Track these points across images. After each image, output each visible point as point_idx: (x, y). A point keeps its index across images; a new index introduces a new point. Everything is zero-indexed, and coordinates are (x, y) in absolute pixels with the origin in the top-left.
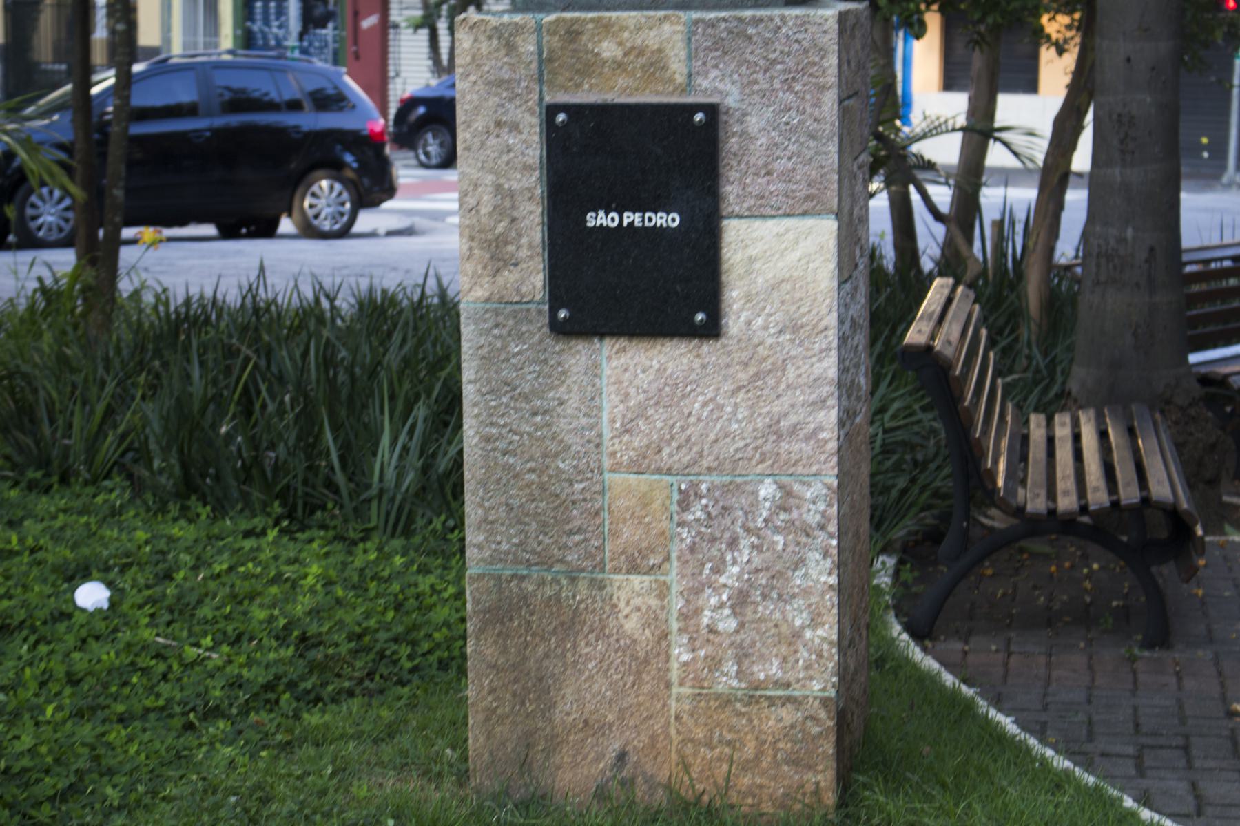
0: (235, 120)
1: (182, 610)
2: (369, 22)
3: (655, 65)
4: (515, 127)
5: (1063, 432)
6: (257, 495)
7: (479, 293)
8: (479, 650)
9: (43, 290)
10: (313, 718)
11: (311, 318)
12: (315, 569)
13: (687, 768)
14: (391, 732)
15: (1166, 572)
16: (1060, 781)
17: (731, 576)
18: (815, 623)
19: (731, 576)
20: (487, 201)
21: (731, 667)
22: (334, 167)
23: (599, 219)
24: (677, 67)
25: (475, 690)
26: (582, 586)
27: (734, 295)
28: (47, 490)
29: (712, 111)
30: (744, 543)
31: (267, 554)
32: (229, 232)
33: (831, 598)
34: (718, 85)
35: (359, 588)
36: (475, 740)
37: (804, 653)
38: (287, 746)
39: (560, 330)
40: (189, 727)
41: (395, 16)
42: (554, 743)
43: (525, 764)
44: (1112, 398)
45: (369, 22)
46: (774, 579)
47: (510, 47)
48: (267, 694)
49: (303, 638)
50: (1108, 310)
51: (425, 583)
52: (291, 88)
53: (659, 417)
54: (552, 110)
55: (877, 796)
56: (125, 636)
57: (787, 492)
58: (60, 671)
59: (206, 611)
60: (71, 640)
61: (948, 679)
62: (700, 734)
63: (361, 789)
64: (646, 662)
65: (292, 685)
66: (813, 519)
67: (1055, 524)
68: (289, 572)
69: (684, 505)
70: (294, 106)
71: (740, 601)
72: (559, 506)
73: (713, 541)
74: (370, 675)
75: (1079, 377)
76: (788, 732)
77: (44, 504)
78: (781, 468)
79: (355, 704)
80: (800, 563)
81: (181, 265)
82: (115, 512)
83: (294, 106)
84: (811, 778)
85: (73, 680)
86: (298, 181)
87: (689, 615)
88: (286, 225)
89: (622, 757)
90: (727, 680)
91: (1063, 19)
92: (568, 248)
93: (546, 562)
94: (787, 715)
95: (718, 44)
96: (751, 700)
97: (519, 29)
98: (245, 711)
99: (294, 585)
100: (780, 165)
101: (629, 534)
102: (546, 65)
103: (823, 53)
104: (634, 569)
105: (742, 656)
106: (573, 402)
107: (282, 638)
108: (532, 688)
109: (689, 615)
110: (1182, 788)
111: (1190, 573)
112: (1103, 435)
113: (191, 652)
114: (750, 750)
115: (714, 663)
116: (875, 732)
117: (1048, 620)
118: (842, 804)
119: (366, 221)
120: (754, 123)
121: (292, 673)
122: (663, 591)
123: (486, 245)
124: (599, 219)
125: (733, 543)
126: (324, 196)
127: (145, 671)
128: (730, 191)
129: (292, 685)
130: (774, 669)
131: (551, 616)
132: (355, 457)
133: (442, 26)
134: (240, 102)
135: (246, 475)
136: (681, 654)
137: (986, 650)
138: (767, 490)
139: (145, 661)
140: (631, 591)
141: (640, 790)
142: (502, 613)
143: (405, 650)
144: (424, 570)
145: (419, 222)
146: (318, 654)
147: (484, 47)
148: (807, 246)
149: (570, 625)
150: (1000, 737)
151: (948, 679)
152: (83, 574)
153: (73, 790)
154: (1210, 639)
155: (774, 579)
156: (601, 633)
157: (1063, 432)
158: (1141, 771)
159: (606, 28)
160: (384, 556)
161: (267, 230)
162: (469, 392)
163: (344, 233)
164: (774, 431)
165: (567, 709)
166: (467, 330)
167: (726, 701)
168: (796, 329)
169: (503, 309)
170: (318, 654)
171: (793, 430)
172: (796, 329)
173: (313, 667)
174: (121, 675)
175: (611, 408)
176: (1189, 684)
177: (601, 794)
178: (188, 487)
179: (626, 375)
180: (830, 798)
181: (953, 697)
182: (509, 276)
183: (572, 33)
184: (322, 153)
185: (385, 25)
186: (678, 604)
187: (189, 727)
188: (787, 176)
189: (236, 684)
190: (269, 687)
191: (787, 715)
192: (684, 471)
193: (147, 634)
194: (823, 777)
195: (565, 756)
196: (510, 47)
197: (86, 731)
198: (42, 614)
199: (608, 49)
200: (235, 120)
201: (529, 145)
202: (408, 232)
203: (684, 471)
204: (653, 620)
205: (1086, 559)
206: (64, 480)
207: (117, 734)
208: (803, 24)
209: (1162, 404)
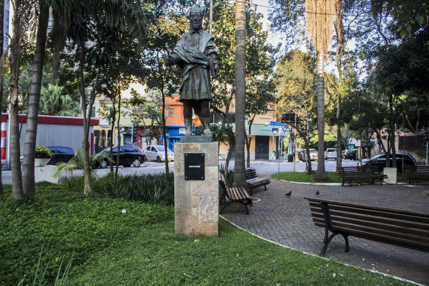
0: (125, 153)
1: (135, 213)
2: (139, 141)
3: (197, 149)
4: (181, 156)
5: (234, 190)
6: (140, 198)
7: (176, 175)
8: (176, 217)
9: (109, 174)
10: (153, 225)
11: (142, 178)
12: (149, 208)
13: (201, 230)
14: (163, 227)
15: (248, 206)
16: (242, 231)
17: (206, 208)
18: (216, 213)
19: (206, 208)
20: (177, 164)
21: (206, 218)
22: (138, 159)
23: (190, 166)
24: (200, 149)
25: (176, 221)
26: (188, 209)
27: (206, 175)
28: (114, 198)
29: (204, 154)
30: (207, 204)
31: (143, 206)
32: (125, 166)
33: (218, 210)
34: (204, 151)
35: (155, 210)
36: (176, 228)
37: (214, 217)
38: (151, 229)
39: (186, 179)
40: (139, 227)
41: (142, 140)
42: (185, 228)
43: (182, 230)
44: (238, 186)
45: (139, 141)
46: (211, 208)
47: (180, 147)
48: (147, 223)
49: (150, 216)
50: (238, 176)
51: (163, 209)
52: (133, 149)
53: (197, 189)
54: (185, 154)
55: (222, 233)
56: (129, 216)
57: (212, 198)
58: (122, 220)
59: (138, 213)
60: (123, 216)
61: (226, 219)
62: (202, 226)
63: (162, 234)
64: (196, 218)
65: (150, 222)
66: (215, 201)
67: (236, 201)
68: (146, 208)
69: (200, 200)
70: (133, 151)
71: (207, 211)
72: (186, 200)
73: (204, 203)
74: (159, 220)
75: (234, 184)
76: (212, 226)
77: (114, 200)
78: (211, 195)
79: (158, 224)
80: (214, 206)
81: (124, 172)
82: (123, 201)
83: (133, 151)
84: (215, 231)
85: (124, 221)
86: (133, 160)
87: (201, 213)
88: (132, 166)
89: (193, 229)
90: (205, 220)
91: (227, 142)
92: (187, 170)
93: (184, 206)
94: (213, 224)
95: (204, 146)
96: (208, 222)
97: (181, 145)
98: (145, 225)
99: (147, 209)
100: (211, 160)
101: (194, 203)
102: (184, 149)
103: (216, 147)
104: (195, 207)
105: (207, 217)
106: (187, 188)
107: (148, 216)
108: (182, 221)
109: (201, 213)
110: (254, 231)
111: (251, 206)
112: (239, 190)
113: (137, 218)
114: (208, 228)
115: (204, 218)
116: (223, 227)
117: (234, 212)
118: (219, 234)
119: (142, 165)
120: (208, 155)
121: (150, 220)
122: (198, 210)
123: (177, 169)
124: (190, 166)
125: (206, 204)
126: (137, 162)
127: (132, 220)
128: (206, 163)
129: (150, 222)
130: (211, 218)
131: (184, 213)
132: (153, 195)
133: (148, 142)
134: (126, 151)
135: (139, 196)
136: (200, 217)
137: (228, 215)
138: (210, 198)
139: (132, 219)
140: (194, 210)
141: (195, 233)
142: (179, 212)
143: (162, 217)
144: (162, 207)
145: (147, 165)
146: (152, 218)
147: (177, 147)
148: (215, 169)
149: (187, 214)
150: (234, 226)
151: (226, 219)
152: (121, 208)
153: (128, 235)
154: (253, 214)
155: (211, 208)
156: (191, 215)
157: (234, 190)
158: (249, 229)
159: (191, 145)
160: (157, 206)
161: (129, 166)
162: (175, 187)
163: (139, 167)
164: (211, 191)
165: (187, 223)
166: (175, 179)
167: (205, 222)
168: (213, 179)
169: (180, 177)
170: (152, 218)
171: (213, 191)
172: (213, 179)
173: (153, 219)
174: (129, 220)
175: (192, 188)
176: (252, 219)
177: (190, 234)
178: (131, 198)
179: (193, 185)
180: (217, 233)
181: (227, 221)
182: (180, 173)
183: (187, 145)
184: (136, 157)
185: (141, 142)
186: (200, 211)
187: (139, 227)
188: (212, 162)
189: (143, 221)
190: (147, 222)
191: (213, 224)
192: (200, 196)
193: (131, 216)
194: (217, 231)
195: (186, 229)
196: (180, 147)
197: (127, 227)
198: (118, 213)
199: (192, 147)
200: (125, 153)
201: (183, 158)
202: (146, 166)
203: (200, 196)
204: (197, 213)
205: (237, 205)
206: (116, 197)
207: (131, 228)
208: (214, 144)
209: (244, 186)
